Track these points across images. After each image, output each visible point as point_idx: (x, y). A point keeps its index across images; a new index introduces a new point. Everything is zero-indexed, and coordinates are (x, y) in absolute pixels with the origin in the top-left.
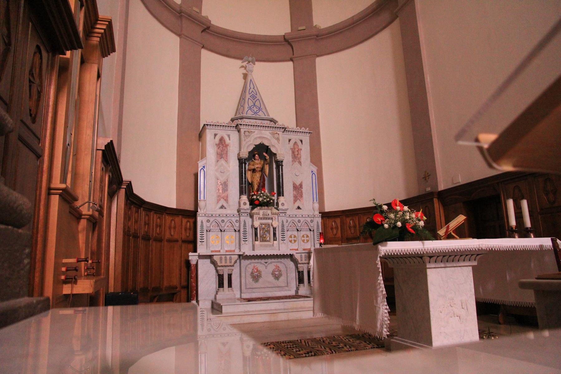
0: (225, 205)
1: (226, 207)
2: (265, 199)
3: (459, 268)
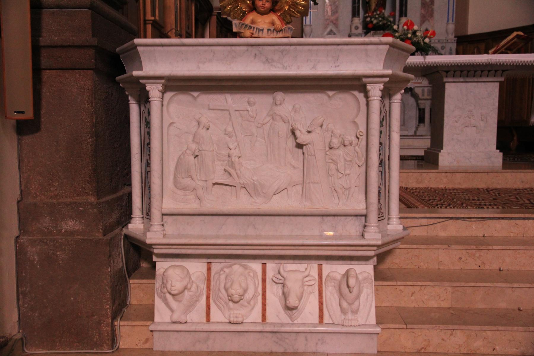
0: (334, 30)
1: (336, 32)
2: (380, 21)
3: (483, 83)
